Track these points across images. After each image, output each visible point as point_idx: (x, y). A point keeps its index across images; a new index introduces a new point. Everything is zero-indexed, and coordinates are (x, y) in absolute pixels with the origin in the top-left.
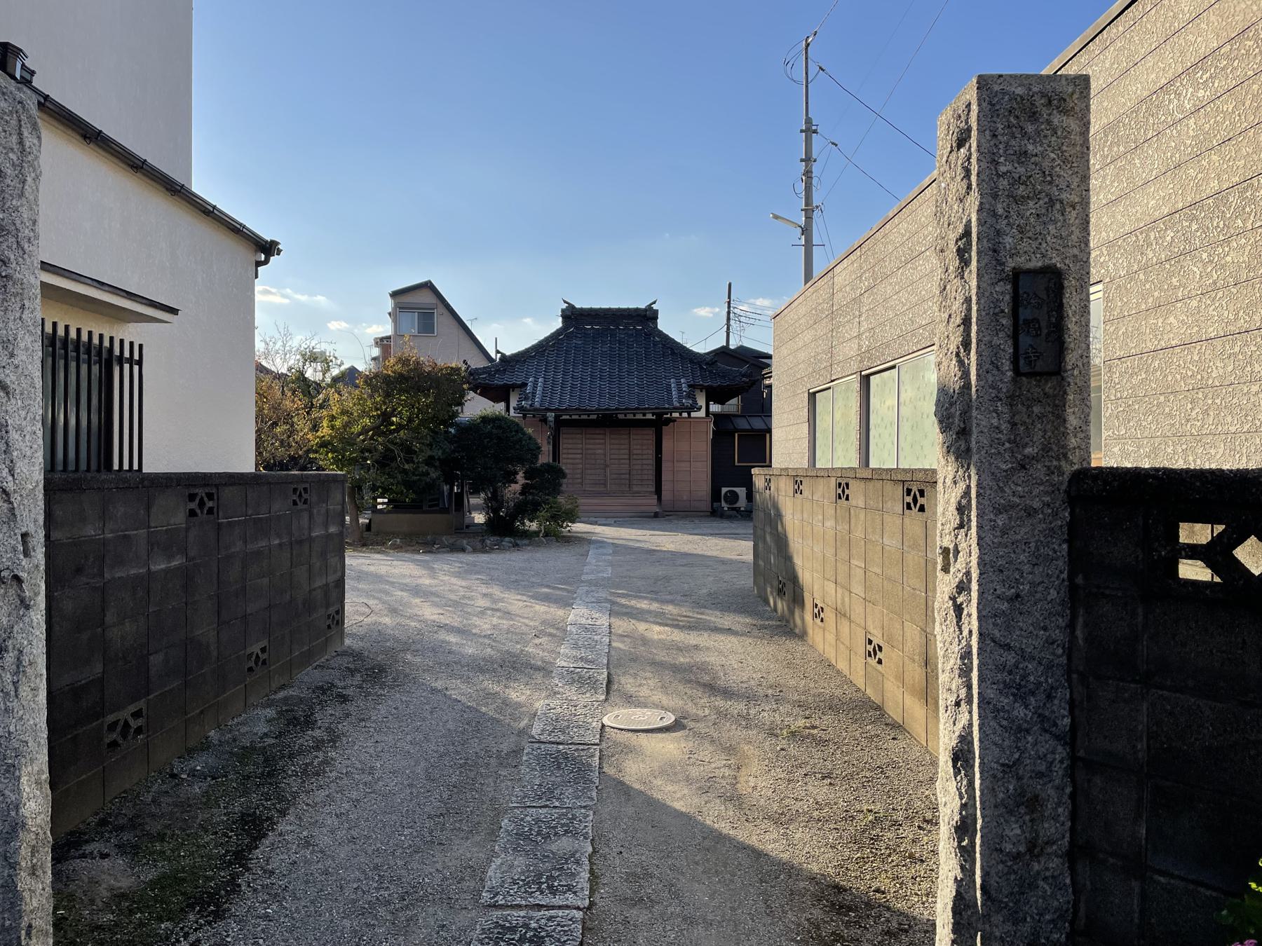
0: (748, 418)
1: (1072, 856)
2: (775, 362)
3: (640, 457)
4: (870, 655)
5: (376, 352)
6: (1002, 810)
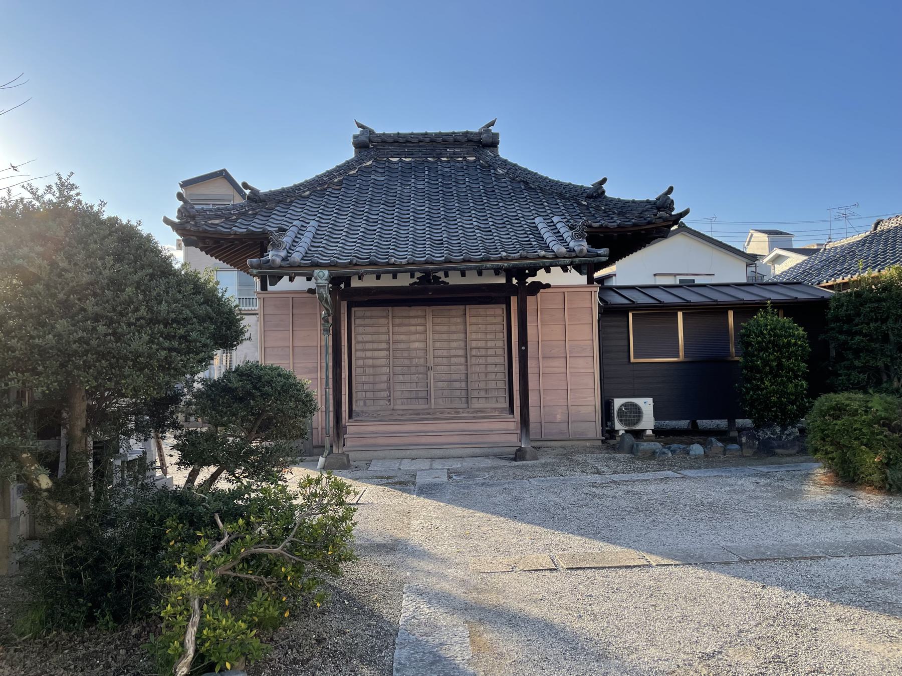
3: (483, 352)
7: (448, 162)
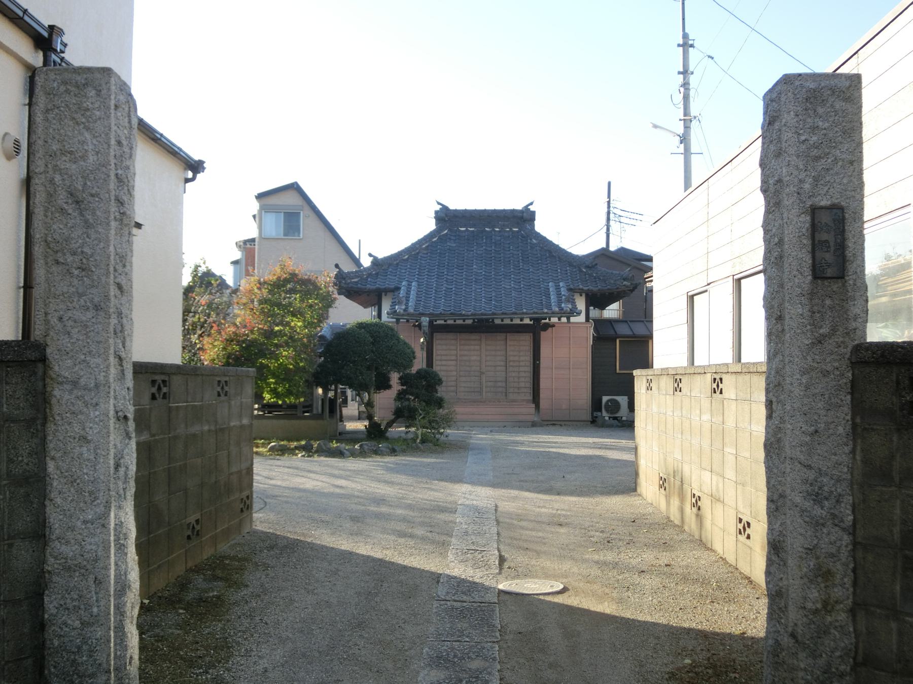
0: (631, 324)
1: (852, 612)
2: (655, 264)
4: (740, 533)
5: (238, 255)
6: (806, 580)
7: (499, 231)
